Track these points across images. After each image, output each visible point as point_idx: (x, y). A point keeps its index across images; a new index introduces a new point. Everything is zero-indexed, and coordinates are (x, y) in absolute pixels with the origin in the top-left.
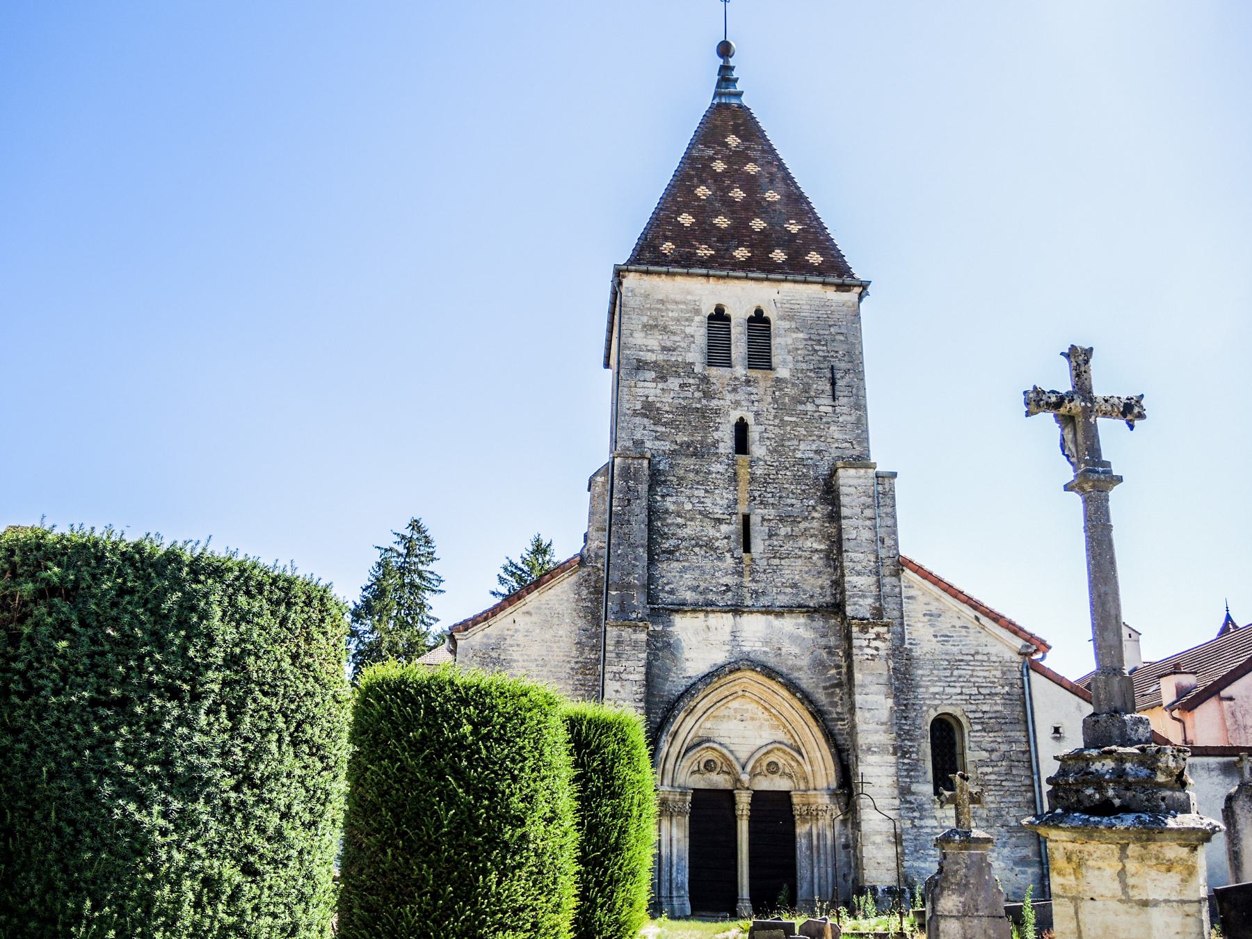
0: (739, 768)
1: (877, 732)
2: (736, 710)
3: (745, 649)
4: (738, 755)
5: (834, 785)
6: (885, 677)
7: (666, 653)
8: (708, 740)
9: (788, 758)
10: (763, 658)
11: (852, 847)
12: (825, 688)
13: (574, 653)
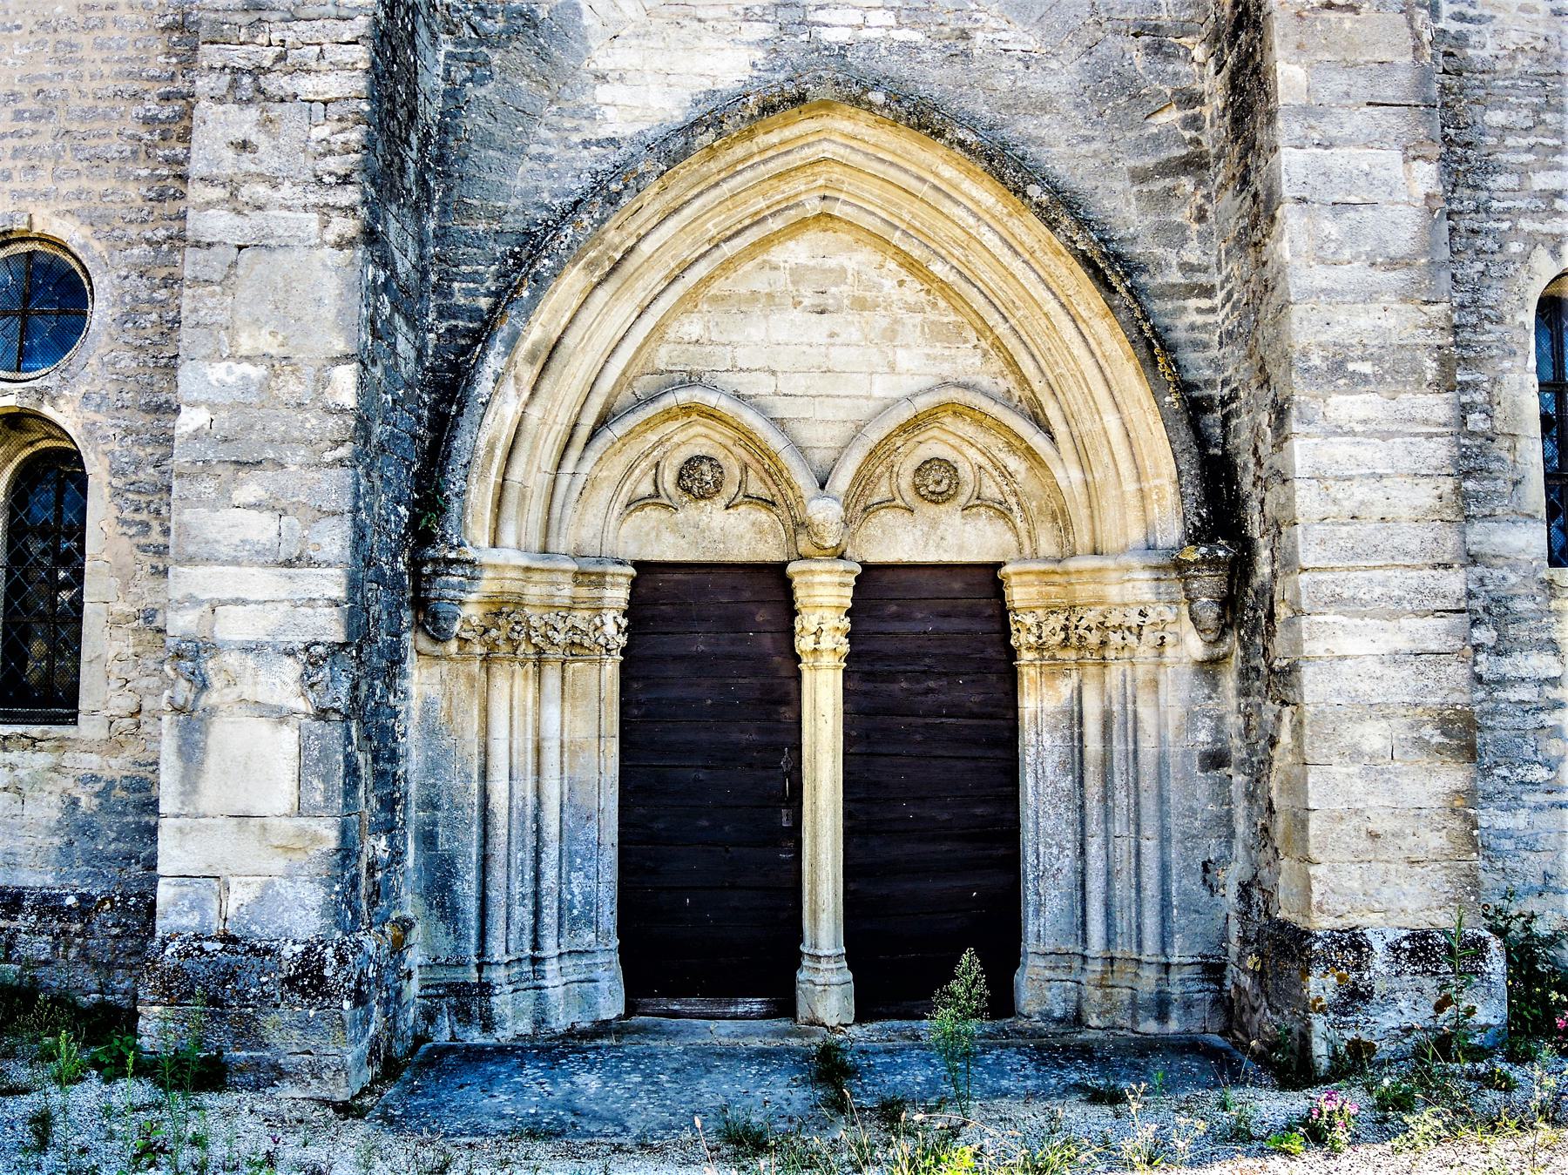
0: (804, 482)
1: (1370, 296)
2: (798, 274)
3: (828, 36)
4: (806, 434)
5: (1171, 532)
6: (1404, 77)
7: (520, 54)
8: (691, 380)
9: (996, 444)
10: (898, 66)
11: (1249, 769)
12: (1140, 176)
13: (159, 62)
